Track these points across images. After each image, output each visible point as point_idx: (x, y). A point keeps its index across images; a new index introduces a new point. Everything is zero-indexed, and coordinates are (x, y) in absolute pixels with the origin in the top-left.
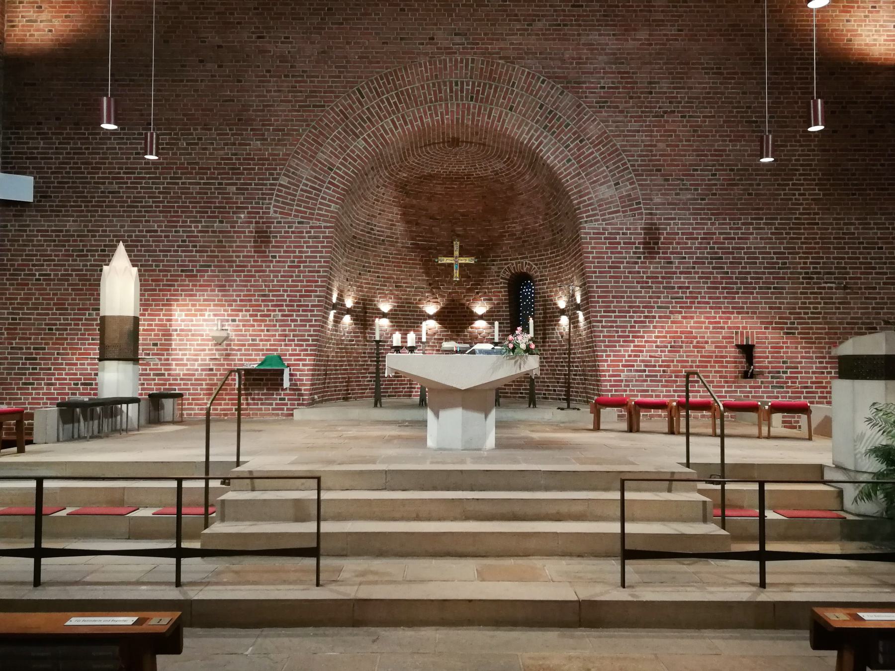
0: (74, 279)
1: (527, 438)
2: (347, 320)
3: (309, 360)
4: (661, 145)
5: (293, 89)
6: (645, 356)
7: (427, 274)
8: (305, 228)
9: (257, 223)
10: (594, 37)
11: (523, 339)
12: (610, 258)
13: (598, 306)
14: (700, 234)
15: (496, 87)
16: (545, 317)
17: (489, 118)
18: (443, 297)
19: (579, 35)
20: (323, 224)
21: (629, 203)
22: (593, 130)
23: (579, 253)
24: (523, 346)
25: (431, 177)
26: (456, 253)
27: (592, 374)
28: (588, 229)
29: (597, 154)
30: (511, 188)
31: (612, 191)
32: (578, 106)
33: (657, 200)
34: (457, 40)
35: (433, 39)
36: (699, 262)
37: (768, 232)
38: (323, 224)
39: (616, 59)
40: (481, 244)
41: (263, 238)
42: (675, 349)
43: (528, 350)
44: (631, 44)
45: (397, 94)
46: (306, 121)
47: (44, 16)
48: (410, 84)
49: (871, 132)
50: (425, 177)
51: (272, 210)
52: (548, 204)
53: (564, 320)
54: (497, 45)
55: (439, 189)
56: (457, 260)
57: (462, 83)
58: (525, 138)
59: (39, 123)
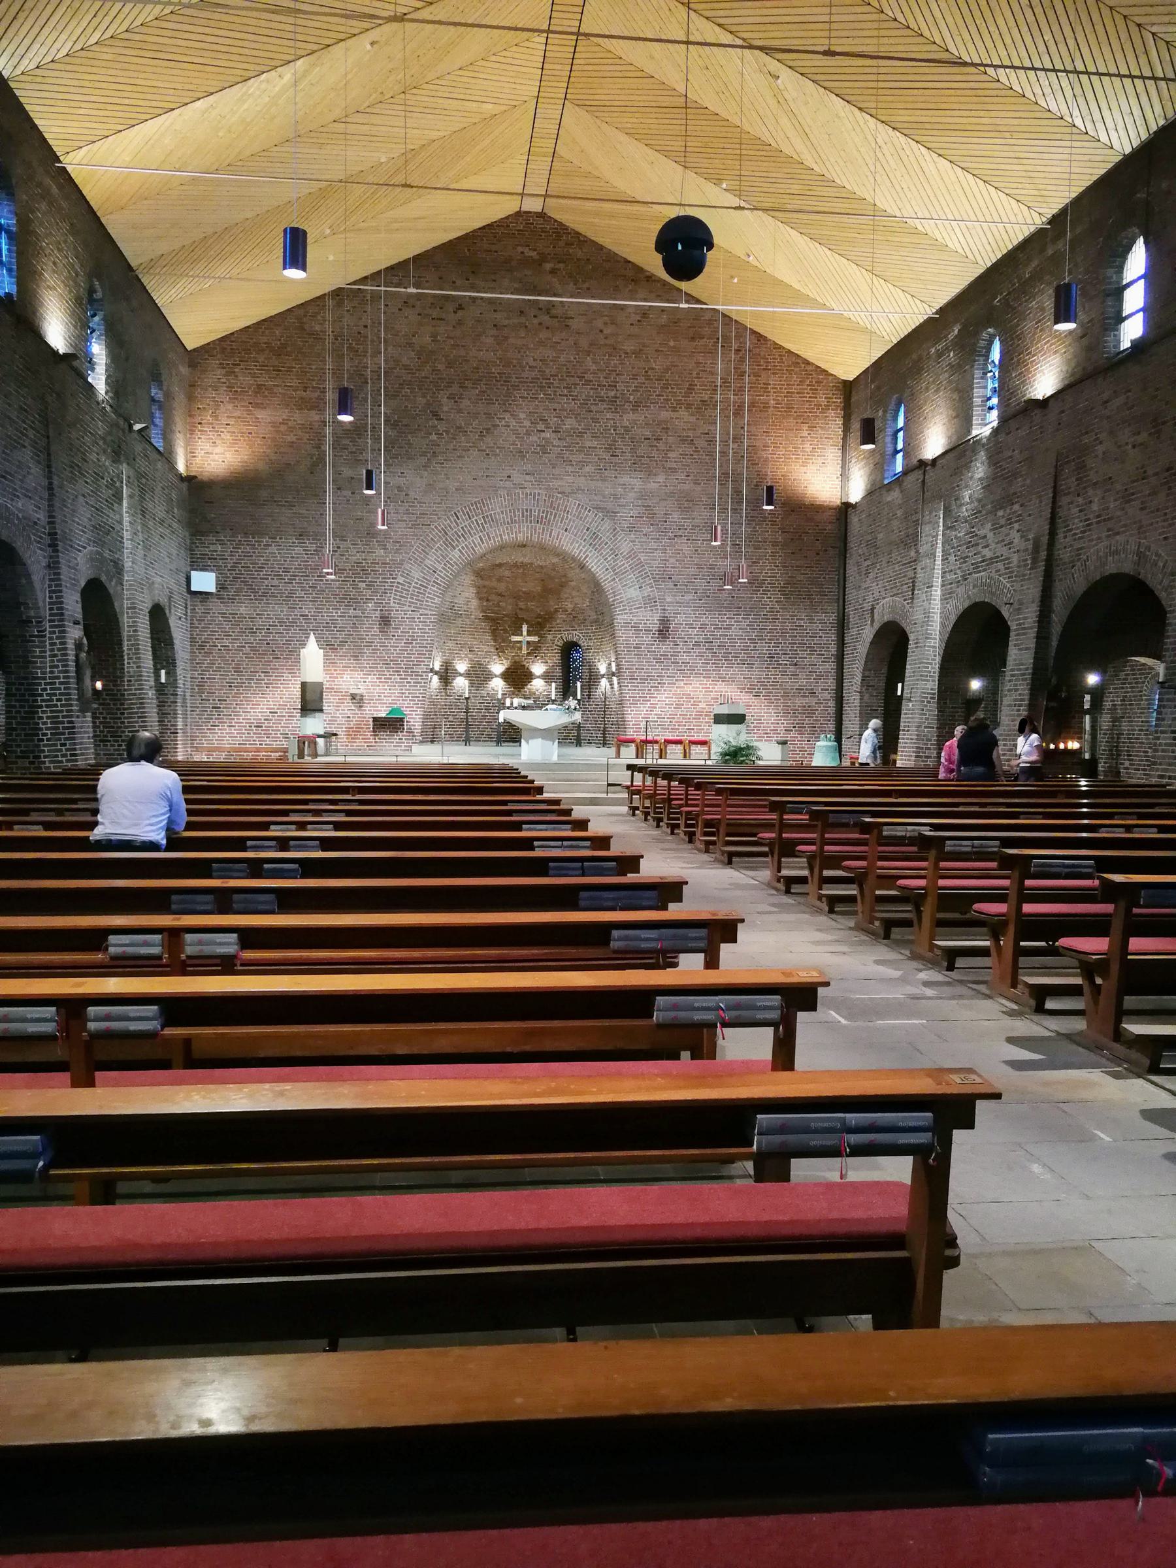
0: (247, 650)
1: (564, 557)
2: (436, 679)
3: (420, 711)
4: (672, 560)
5: (407, 512)
6: (657, 711)
7: (495, 641)
8: (416, 615)
9: (381, 610)
10: (626, 479)
11: (572, 703)
12: (634, 641)
13: (626, 675)
14: (697, 625)
15: (556, 514)
16: (590, 679)
17: (550, 536)
18: (508, 659)
19: (616, 477)
20: (430, 613)
21: (650, 602)
22: (625, 547)
23: (613, 636)
24: (573, 707)
25: (500, 565)
26: (525, 633)
27: (621, 723)
28: (620, 619)
29: (627, 565)
30: (565, 576)
31: (638, 593)
32: (614, 530)
33: (669, 599)
34: (528, 478)
35: (509, 477)
36: (697, 644)
37: (744, 624)
38: (430, 613)
39: (643, 496)
40: (539, 616)
41: (385, 621)
42: (678, 706)
43: (575, 709)
44: (653, 486)
45: (483, 517)
46: (416, 535)
47: (219, 449)
48: (493, 510)
49: (818, 554)
50: (497, 565)
51: (392, 602)
52: (593, 592)
53: (604, 682)
54: (556, 483)
55: (507, 573)
56: (524, 637)
57: (531, 510)
58: (576, 552)
59: (217, 532)
